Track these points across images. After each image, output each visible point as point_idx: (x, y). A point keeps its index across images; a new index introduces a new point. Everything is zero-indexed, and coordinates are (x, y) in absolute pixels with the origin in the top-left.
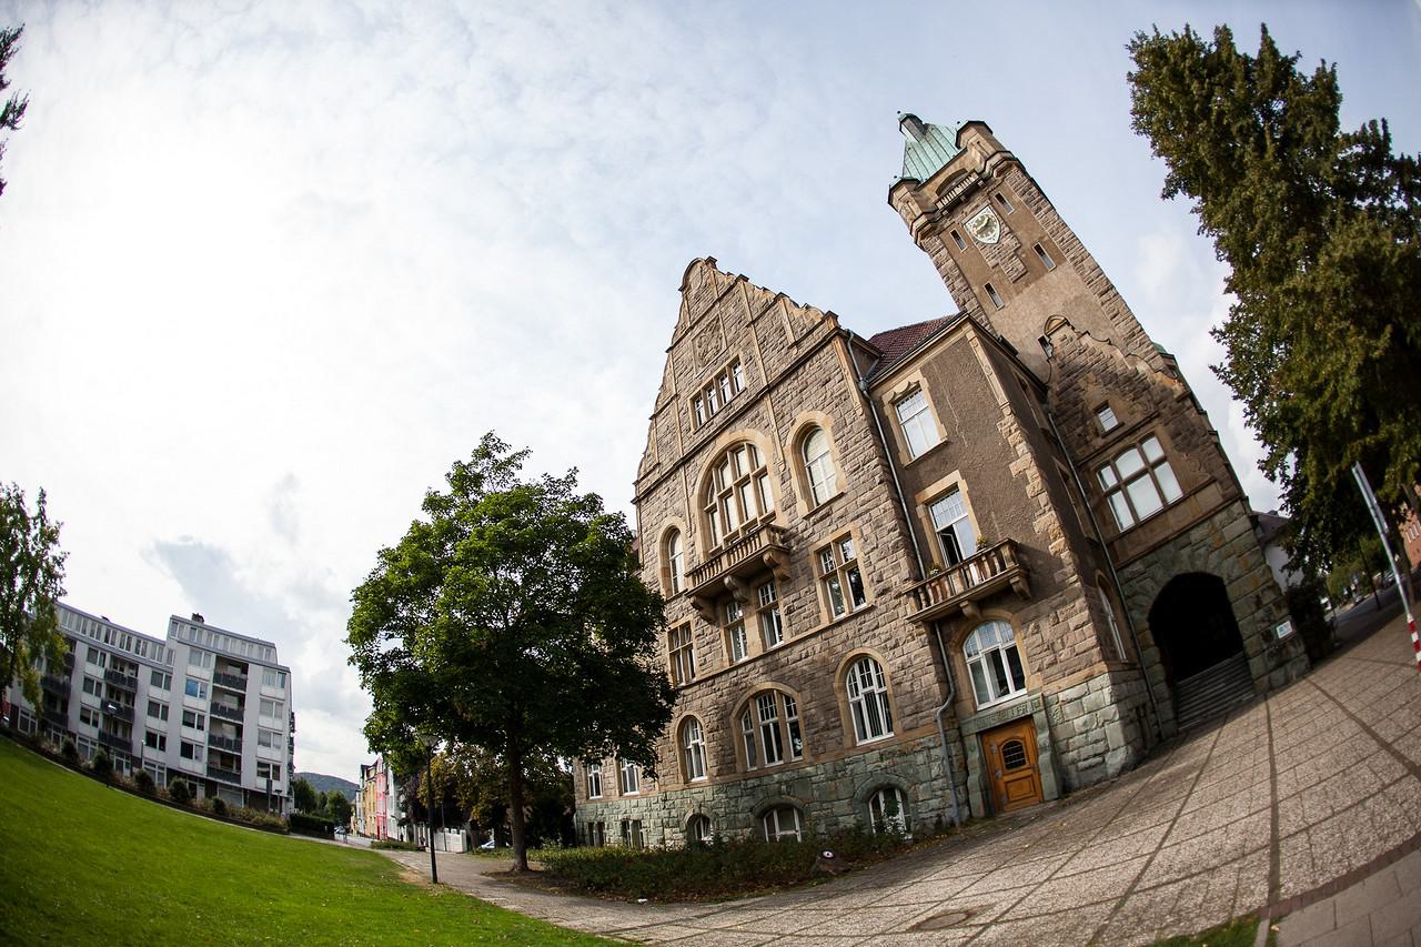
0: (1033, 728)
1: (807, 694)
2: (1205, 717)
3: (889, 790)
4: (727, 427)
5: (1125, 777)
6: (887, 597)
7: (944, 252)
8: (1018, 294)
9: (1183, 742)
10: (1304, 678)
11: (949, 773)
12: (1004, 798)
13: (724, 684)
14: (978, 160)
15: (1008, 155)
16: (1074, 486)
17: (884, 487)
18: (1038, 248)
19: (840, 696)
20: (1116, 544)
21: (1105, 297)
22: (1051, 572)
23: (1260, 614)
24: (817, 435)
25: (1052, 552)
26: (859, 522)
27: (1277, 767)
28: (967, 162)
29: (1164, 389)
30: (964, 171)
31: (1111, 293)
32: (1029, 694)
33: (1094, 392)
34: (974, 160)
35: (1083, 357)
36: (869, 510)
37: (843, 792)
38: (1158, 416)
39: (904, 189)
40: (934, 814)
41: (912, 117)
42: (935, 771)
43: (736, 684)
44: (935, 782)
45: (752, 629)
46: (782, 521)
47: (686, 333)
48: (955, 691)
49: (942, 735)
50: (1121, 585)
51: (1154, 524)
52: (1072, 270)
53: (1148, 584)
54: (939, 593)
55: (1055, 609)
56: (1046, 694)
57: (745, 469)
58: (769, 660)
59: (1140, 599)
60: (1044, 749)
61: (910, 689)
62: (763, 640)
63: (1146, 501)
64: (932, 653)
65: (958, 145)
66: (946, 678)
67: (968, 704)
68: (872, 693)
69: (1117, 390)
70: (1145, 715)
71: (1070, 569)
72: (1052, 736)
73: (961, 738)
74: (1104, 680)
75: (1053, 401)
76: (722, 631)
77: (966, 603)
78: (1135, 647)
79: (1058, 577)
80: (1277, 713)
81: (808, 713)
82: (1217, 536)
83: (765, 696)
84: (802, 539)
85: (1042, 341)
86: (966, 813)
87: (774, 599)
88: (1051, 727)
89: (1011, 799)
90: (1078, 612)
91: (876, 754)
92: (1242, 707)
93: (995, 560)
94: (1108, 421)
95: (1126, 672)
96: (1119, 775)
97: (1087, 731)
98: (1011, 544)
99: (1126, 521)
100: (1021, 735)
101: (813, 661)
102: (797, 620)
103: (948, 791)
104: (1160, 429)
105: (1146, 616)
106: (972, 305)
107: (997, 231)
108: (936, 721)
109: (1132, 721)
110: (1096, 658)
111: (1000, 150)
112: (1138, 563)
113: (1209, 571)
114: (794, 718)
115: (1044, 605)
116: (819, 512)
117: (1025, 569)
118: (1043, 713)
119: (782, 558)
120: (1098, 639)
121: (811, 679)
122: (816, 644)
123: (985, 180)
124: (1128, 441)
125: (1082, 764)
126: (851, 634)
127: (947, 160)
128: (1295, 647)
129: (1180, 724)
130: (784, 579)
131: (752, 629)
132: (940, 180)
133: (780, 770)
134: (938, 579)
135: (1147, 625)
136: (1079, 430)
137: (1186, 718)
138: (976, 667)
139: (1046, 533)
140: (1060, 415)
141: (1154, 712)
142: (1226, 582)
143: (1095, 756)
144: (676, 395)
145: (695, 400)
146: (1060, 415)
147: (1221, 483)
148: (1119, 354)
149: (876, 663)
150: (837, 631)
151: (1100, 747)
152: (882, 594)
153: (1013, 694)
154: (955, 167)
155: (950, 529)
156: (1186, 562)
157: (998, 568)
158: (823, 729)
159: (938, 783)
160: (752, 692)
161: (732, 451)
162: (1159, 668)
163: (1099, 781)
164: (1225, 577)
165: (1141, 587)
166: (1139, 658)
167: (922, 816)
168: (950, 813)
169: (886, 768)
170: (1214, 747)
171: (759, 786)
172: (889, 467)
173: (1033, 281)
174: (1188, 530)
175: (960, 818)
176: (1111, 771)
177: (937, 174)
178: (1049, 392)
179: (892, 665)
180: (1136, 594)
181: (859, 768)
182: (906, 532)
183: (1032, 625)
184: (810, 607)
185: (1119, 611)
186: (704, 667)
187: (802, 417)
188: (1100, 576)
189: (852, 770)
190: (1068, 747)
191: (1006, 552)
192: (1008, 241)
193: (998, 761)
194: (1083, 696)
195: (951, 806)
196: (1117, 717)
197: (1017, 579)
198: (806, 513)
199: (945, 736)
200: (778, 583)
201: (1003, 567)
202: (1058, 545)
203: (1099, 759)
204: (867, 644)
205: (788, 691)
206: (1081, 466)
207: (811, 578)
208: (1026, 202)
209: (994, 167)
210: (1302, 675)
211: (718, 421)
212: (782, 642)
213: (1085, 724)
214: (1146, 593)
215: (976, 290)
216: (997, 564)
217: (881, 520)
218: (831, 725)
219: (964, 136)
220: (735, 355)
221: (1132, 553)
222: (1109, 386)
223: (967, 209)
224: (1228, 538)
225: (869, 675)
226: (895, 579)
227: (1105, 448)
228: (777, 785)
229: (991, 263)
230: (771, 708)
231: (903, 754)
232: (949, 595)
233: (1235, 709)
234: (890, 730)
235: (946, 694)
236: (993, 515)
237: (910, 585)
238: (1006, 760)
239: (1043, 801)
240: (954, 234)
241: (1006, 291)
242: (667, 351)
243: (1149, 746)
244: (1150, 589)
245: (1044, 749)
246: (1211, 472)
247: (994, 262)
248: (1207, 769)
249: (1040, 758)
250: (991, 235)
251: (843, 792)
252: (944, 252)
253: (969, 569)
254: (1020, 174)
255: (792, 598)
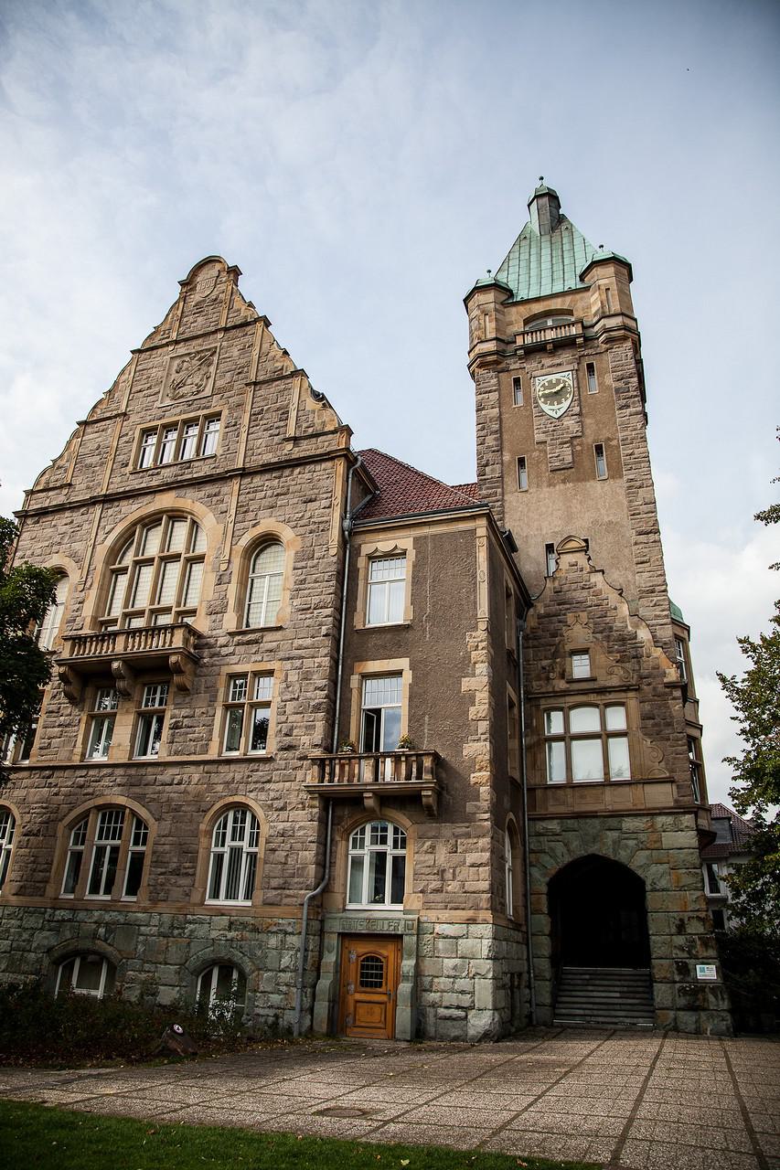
0: (400, 950)
1: (166, 825)
2: (589, 1022)
3: (227, 967)
4: (174, 488)
5: (484, 1045)
6: (289, 754)
7: (494, 396)
8: (549, 486)
9: (556, 1037)
10: (720, 1039)
11: (300, 971)
12: (350, 1019)
13: (65, 781)
14: (594, 310)
15: (631, 323)
16: (517, 717)
17: (328, 642)
18: (599, 449)
19: (203, 840)
20: (539, 793)
21: (643, 538)
22: (466, 799)
23: (680, 940)
24: (274, 548)
25: (473, 781)
26: (288, 665)
27: (645, 1096)
28: (580, 305)
29: (657, 667)
30: (570, 312)
31: (652, 537)
32: (405, 912)
33: (578, 633)
34: (589, 307)
35: (585, 593)
36: (303, 657)
37: (175, 954)
38: (636, 690)
39: (490, 297)
40: (271, 1012)
41: (552, 197)
42: (286, 961)
43: (81, 787)
44: (281, 974)
45: (124, 729)
46: (201, 624)
47: (167, 345)
48: (329, 878)
49: (305, 923)
50: (529, 836)
51: (586, 792)
52: (622, 492)
53: (560, 848)
54: (346, 774)
55: (457, 837)
56: (422, 919)
57: (179, 544)
58: (133, 771)
59: (545, 859)
60: (406, 978)
61: (283, 860)
62: (132, 747)
63: (587, 764)
64: (319, 830)
65: (582, 278)
66: (325, 863)
67: (339, 898)
68: (240, 850)
69: (605, 644)
70: (519, 987)
71: (485, 805)
72: (417, 966)
73: (321, 933)
74: (486, 930)
75: (532, 621)
76: (84, 718)
77: (371, 795)
78: (526, 907)
79: (470, 807)
80: (668, 1056)
81: (160, 848)
82: (655, 837)
83: (113, 813)
84: (218, 654)
85: (550, 548)
86: (307, 1022)
87: (160, 704)
88: (419, 958)
89: (358, 1023)
90: (479, 851)
91: (224, 921)
92: (632, 1032)
93: (414, 766)
94: (580, 668)
95: (511, 930)
96: (479, 1041)
97: (455, 977)
98: (436, 756)
99: (557, 776)
100: (385, 953)
101: (185, 792)
102: (181, 739)
103: (294, 990)
104: (633, 703)
105: (547, 879)
106: (493, 470)
107: (565, 405)
108: (303, 905)
109: (503, 987)
110: (484, 904)
111: (627, 313)
112: (555, 822)
113: (632, 866)
114: (140, 848)
115: (447, 829)
116: (247, 636)
117: (440, 786)
118: (415, 938)
119: (189, 666)
120: (492, 885)
121: (176, 810)
122: (195, 774)
123: (587, 339)
124: (592, 698)
125: (442, 1011)
126: (238, 777)
127: (558, 288)
128: (716, 997)
129: (556, 1016)
130: (183, 689)
131: (124, 729)
132: (537, 308)
133: (105, 907)
134: (350, 759)
135: (544, 889)
136: (545, 663)
137: (563, 1011)
138: (357, 863)
139: (473, 760)
140: (531, 639)
141: (529, 987)
142: (648, 888)
143: (458, 1007)
144: (125, 414)
145: (147, 432)
146: (531, 639)
147: (678, 787)
148: (624, 610)
149: (254, 817)
150: (223, 768)
151: (465, 1000)
152: (286, 749)
153: (388, 905)
154: (563, 303)
155: (378, 711)
156: (607, 846)
157: (414, 774)
158: (171, 873)
159: (286, 977)
160: (100, 801)
161: (170, 518)
162: (545, 940)
163: (456, 1039)
164: (648, 882)
165: (551, 848)
166: (526, 920)
167: (258, 1011)
168: (290, 1017)
169: (232, 940)
170: (589, 1055)
171: (69, 920)
172: (340, 622)
173: (573, 481)
174: (623, 816)
175: (300, 1027)
176: (472, 1032)
177: (537, 300)
178: (532, 610)
179: (271, 827)
180: (543, 852)
181: (201, 931)
182: (333, 697)
183: (428, 844)
184: (200, 731)
185: (519, 861)
186: (44, 752)
187: (267, 524)
188: (511, 820)
189: (192, 931)
190: (431, 986)
191: (427, 763)
192: (570, 423)
193: (353, 973)
194: (461, 937)
195: (293, 1009)
196: (490, 975)
197: (430, 793)
198: (233, 628)
199: (307, 924)
200: (173, 689)
201: (419, 776)
202: (481, 778)
203: (461, 1013)
204: (252, 795)
205: (143, 813)
206: (532, 699)
207: (213, 699)
208: (617, 390)
209: (607, 330)
210: (719, 1035)
211: (168, 475)
212: (156, 757)
213: (455, 968)
214: (554, 857)
215: (507, 457)
216: (414, 770)
217: (312, 674)
218: (184, 871)
219: (597, 271)
220: (218, 409)
221: (552, 809)
222: (599, 636)
223: (547, 361)
224: (665, 844)
225: (242, 829)
226: (305, 739)
227: (565, 693)
228: (94, 926)
229: (539, 437)
230: (115, 828)
231: (256, 930)
232: (356, 779)
233: (626, 1030)
234: (247, 897)
235: (320, 878)
236: (426, 718)
237: (318, 753)
238: (362, 975)
239: (393, 1037)
240: (517, 381)
241: (538, 476)
242: (133, 352)
243: (516, 1023)
244: (559, 854)
245: (406, 978)
246: (672, 771)
247: (541, 437)
248: (576, 1071)
249: (400, 986)
250: (556, 407)
251: (175, 954)
252: (494, 396)
253: (384, 762)
254: (630, 354)
255: (184, 712)
